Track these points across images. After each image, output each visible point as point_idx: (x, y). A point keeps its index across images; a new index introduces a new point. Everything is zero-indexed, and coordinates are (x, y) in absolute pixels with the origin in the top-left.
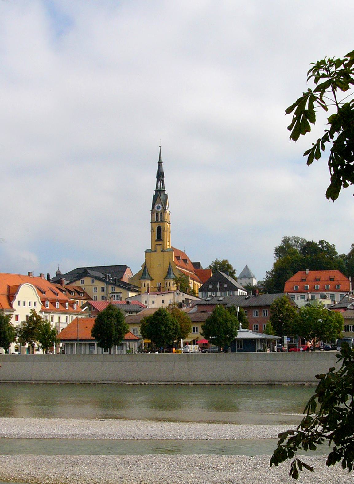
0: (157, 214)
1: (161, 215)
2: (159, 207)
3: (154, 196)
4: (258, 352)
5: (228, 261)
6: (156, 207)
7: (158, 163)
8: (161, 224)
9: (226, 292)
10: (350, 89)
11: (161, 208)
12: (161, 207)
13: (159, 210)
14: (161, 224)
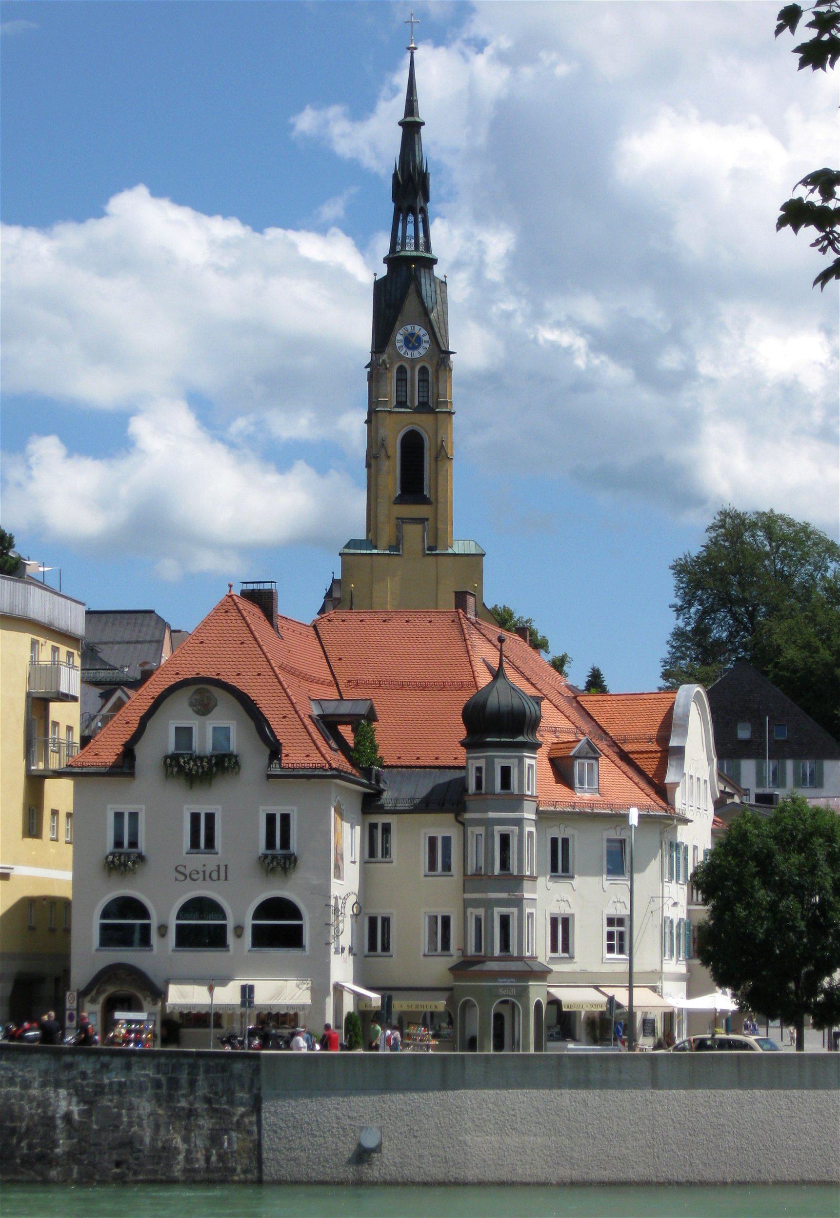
0: (401, 370)
2: (412, 342)
3: (380, 287)
6: (399, 337)
8: (423, 423)
11: (427, 345)
12: (426, 338)
13: (416, 354)
14: (423, 423)
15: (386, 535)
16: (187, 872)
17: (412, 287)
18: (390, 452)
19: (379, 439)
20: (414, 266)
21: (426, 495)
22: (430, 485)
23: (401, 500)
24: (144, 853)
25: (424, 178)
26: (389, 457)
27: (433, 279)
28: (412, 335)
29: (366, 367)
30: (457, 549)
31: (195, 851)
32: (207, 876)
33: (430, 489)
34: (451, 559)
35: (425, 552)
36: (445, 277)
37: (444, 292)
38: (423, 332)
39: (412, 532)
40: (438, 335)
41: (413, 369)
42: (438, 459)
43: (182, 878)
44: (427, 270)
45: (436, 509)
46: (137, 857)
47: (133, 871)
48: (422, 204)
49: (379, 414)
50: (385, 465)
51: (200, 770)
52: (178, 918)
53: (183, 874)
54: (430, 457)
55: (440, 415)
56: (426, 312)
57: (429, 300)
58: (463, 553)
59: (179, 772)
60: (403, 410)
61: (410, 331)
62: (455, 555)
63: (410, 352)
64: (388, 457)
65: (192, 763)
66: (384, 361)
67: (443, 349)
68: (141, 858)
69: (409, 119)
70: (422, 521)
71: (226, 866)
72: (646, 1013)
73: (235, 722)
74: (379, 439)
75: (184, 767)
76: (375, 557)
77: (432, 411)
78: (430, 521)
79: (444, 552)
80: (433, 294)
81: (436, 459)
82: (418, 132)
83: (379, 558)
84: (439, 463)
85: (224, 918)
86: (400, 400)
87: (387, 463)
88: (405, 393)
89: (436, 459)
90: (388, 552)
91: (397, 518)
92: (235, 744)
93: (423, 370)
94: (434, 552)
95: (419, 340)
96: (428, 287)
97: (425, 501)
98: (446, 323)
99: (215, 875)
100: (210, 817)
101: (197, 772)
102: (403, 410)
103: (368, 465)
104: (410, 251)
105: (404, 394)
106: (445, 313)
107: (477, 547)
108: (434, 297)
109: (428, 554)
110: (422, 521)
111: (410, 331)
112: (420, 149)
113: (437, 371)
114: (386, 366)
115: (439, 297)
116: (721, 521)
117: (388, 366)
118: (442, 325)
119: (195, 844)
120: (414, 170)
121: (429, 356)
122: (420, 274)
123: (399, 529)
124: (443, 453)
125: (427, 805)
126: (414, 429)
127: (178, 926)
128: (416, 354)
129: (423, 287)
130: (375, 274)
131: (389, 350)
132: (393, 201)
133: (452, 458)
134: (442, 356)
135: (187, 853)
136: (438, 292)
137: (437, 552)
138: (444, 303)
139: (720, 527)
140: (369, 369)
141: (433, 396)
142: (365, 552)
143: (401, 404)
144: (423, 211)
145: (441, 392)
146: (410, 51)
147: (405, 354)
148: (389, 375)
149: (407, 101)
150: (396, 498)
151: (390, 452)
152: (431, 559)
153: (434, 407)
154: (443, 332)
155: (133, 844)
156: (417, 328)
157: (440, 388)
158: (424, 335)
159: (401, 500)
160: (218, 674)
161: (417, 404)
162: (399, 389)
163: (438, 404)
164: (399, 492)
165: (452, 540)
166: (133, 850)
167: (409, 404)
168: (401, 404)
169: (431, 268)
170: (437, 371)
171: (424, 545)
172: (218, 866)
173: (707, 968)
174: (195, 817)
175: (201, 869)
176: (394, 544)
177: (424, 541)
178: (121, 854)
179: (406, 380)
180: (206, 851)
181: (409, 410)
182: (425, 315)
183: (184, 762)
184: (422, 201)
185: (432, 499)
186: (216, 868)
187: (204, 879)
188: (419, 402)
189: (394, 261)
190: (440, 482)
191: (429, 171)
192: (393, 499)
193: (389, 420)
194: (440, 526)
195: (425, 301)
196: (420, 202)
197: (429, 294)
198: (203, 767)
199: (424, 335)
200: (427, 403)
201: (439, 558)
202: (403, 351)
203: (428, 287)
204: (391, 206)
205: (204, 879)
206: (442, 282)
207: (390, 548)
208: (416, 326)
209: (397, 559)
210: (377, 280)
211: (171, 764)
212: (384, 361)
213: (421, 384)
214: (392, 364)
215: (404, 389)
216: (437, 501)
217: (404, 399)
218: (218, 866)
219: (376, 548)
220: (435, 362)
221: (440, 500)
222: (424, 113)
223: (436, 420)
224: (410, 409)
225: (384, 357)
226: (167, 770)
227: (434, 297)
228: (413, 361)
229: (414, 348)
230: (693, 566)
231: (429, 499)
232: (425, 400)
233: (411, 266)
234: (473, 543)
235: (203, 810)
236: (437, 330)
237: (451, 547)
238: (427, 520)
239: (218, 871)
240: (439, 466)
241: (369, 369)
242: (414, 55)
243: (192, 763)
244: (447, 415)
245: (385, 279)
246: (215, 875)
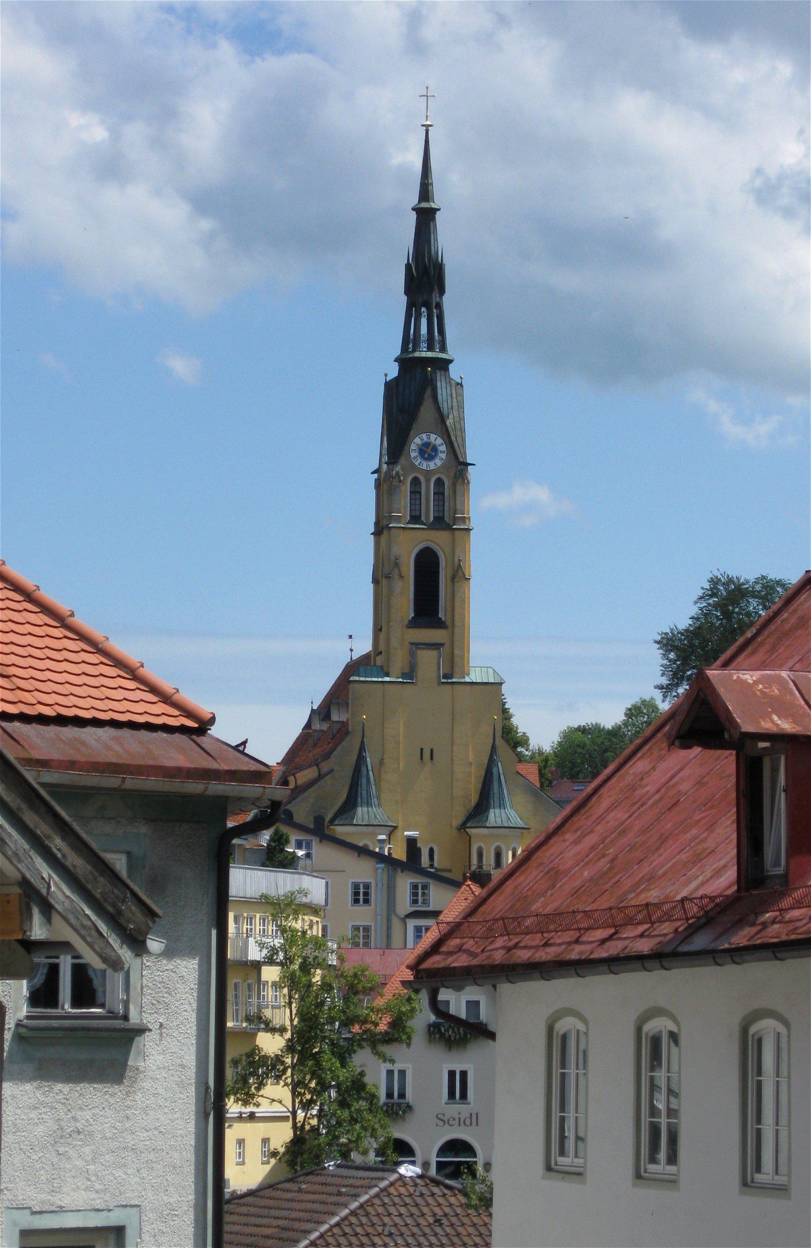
0: (416, 482)
1: (440, 493)
2: (428, 452)
3: (392, 389)
4: (661, 1118)
5: (625, 713)
6: (413, 447)
7: (413, 216)
8: (438, 540)
9: (228, 1118)
10: (439, 210)
11: (443, 456)
12: (443, 448)
13: (432, 465)
14: (438, 540)
15: (399, 661)
16: (446, 1119)
17: (428, 392)
18: (404, 570)
19: (393, 558)
20: (430, 369)
21: (441, 619)
22: (445, 607)
24: (411, 1104)
25: (439, 269)
26: (402, 577)
27: (449, 380)
29: (373, 473)
30: (474, 676)
31: (451, 1101)
32: (461, 1122)
33: (446, 611)
34: (468, 687)
35: (440, 680)
36: (461, 378)
37: (460, 396)
38: (439, 441)
39: (427, 658)
40: (455, 445)
41: (428, 481)
42: (456, 580)
43: (442, 1123)
44: (443, 373)
45: (453, 633)
46: (406, 1107)
47: (403, 1118)
48: (438, 300)
49: (393, 531)
50: (398, 585)
51: (458, 1037)
52: (437, 1156)
53: (443, 1120)
54: (446, 578)
55: (456, 532)
56: (442, 418)
57: (445, 404)
58: (481, 681)
59: (440, 1038)
60: (418, 526)
62: (472, 683)
64: (401, 577)
65: (450, 1031)
66: (397, 473)
67: (461, 460)
68: (409, 1107)
69: (424, 205)
70: (436, 646)
71: (477, 1114)
73: (484, 997)
74: (393, 558)
75: (445, 1034)
76: (386, 686)
77: (449, 528)
78: (445, 646)
79: (461, 680)
80: (449, 397)
81: (453, 578)
82: (434, 219)
83: (392, 686)
84: (456, 584)
85: (475, 1156)
86: (414, 514)
87: (400, 583)
89: (453, 578)
90: (401, 680)
91: (411, 644)
92: (484, 1015)
93: (439, 482)
94: (450, 681)
95: (435, 449)
96: (444, 390)
97: (440, 624)
98: (463, 430)
99: (468, 1121)
100: (464, 1074)
101: (455, 1038)
102: (418, 526)
103: (376, 581)
104: (423, 353)
105: (418, 507)
106: (462, 419)
107: (496, 675)
108: (449, 401)
109: (443, 682)
110: (436, 646)
112: (436, 238)
113: (454, 485)
114: (400, 479)
115: (455, 400)
116: (711, 589)
117: (402, 478)
118: (459, 433)
119: (452, 1094)
120: (429, 262)
121: (445, 467)
122: (436, 377)
123: (413, 655)
124: (460, 573)
126: (428, 545)
127: (437, 1162)
128: (432, 465)
129: (439, 391)
130: (386, 375)
131: (402, 460)
132: (406, 293)
133: (469, 579)
134: (460, 467)
135: (446, 1104)
136: (454, 395)
137: (454, 680)
138: (461, 407)
139: (711, 596)
140: (376, 476)
141: (449, 510)
142: (375, 679)
143: (415, 519)
144: (439, 306)
145: (458, 507)
146: (425, 128)
147: (419, 464)
148: (403, 488)
149: (421, 184)
150: (410, 621)
151: (404, 573)
152: (448, 687)
153: (451, 524)
154: (459, 440)
155: (402, 1095)
156: (433, 437)
157: (458, 502)
158: (442, 452)
161: (432, 519)
162: (413, 501)
163: (455, 520)
165: (469, 666)
166: (401, 1101)
167: (423, 518)
168: (415, 519)
169: (446, 369)
170: (454, 485)
171: (440, 672)
172: (471, 1114)
174: (452, 1074)
175: (457, 1116)
176: (407, 670)
177: (439, 668)
178: (393, 1104)
179: (420, 493)
180: (460, 1102)
181: (424, 527)
182: (441, 424)
183: (445, 1030)
184: (438, 295)
185: (448, 623)
186: (469, 1116)
187: (459, 1125)
188: (434, 517)
189: (406, 363)
190: (457, 604)
191: (444, 262)
192: (406, 622)
193: (402, 537)
194: (456, 652)
195: (441, 406)
196: (435, 298)
197: (445, 399)
198: (460, 1034)
199: (442, 452)
200: (443, 518)
201: (455, 686)
202: (419, 462)
203: (444, 390)
204: (404, 299)
205: (459, 1125)
206: (458, 384)
207: (403, 675)
208: (432, 435)
209: (409, 686)
210: (387, 380)
211: (433, 1032)
212: (397, 473)
213: (437, 496)
214: (405, 476)
215: (418, 502)
216: (453, 625)
217: (418, 514)
218: (471, 1114)
219: (387, 675)
220: (452, 474)
221: (457, 623)
222: (439, 200)
223: (454, 536)
224: (425, 524)
225: (398, 468)
226: (431, 1037)
227: (449, 401)
228: (428, 474)
229: (431, 458)
230: (680, 640)
231: (444, 622)
232: (441, 515)
233: (426, 369)
234: (491, 671)
235: (458, 1068)
236: (453, 438)
237: (468, 674)
238: (442, 645)
239: (471, 1118)
240: (456, 588)
241: (376, 476)
242: (430, 133)
243: (450, 1031)
245: (396, 379)
246: (468, 1121)
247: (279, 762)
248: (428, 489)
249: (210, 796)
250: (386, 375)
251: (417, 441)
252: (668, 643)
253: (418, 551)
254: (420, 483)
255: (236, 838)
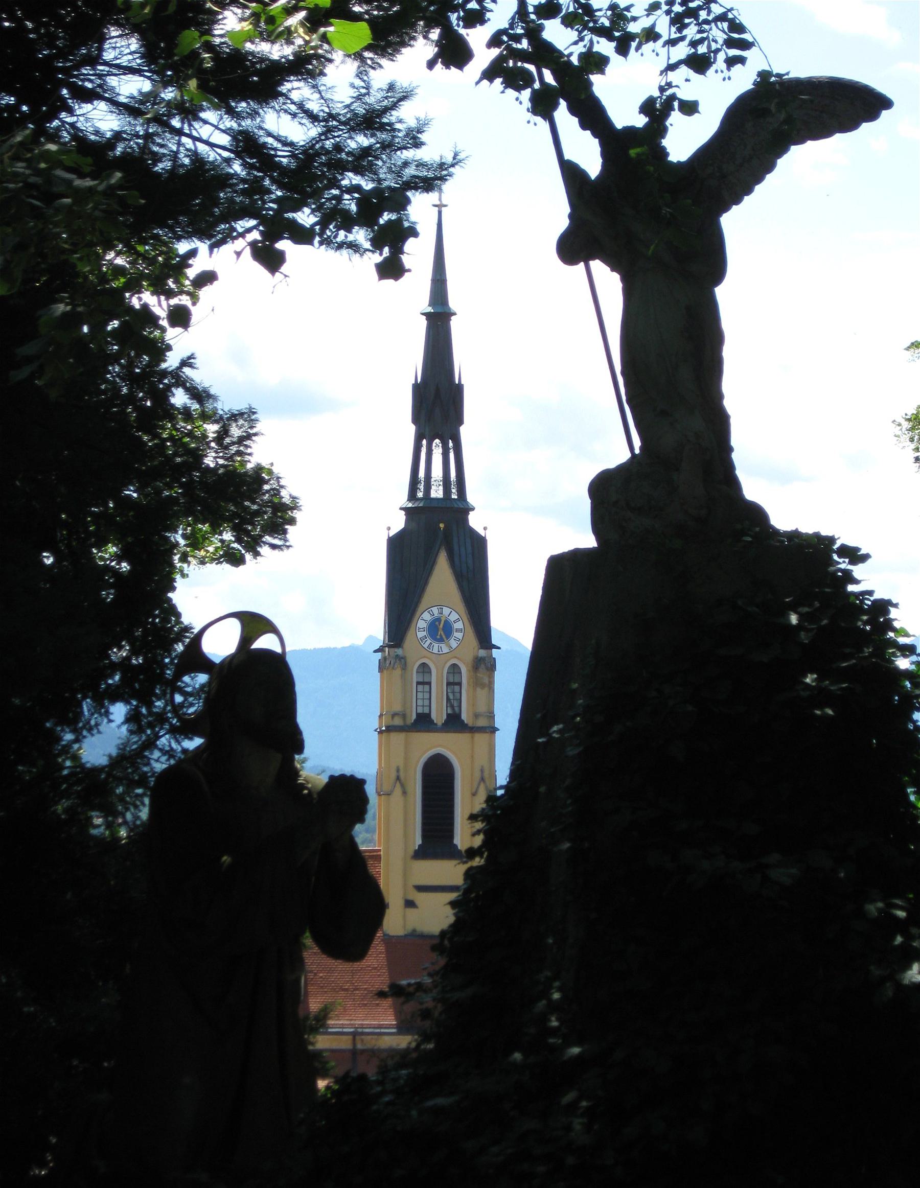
6: (421, 624)
23: (421, 854)
25: (457, 391)
28: (441, 640)
36: (485, 529)
61: (436, 615)
63: (436, 645)
72: (378, 858)
88: (428, 701)
95: (448, 629)
111: (436, 615)
125: (404, 669)
130: (389, 529)
140: (379, 655)
146: (437, 209)
158: (457, 630)
159: (421, 854)
160: (377, 1005)
164: (419, 841)
173: (176, 578)
199: (457, 630)
204: (412, 429)
210: (390, 536)
241: (379, 655)
244: (474, 790)
247: (739, 65)
248: (438, 678)
249: (896, 937)
250: (389, 529)
251: (427, 616)
252: (797, 529)
253: (426, 760)
254: (430, 672)
255: (358, 823)
